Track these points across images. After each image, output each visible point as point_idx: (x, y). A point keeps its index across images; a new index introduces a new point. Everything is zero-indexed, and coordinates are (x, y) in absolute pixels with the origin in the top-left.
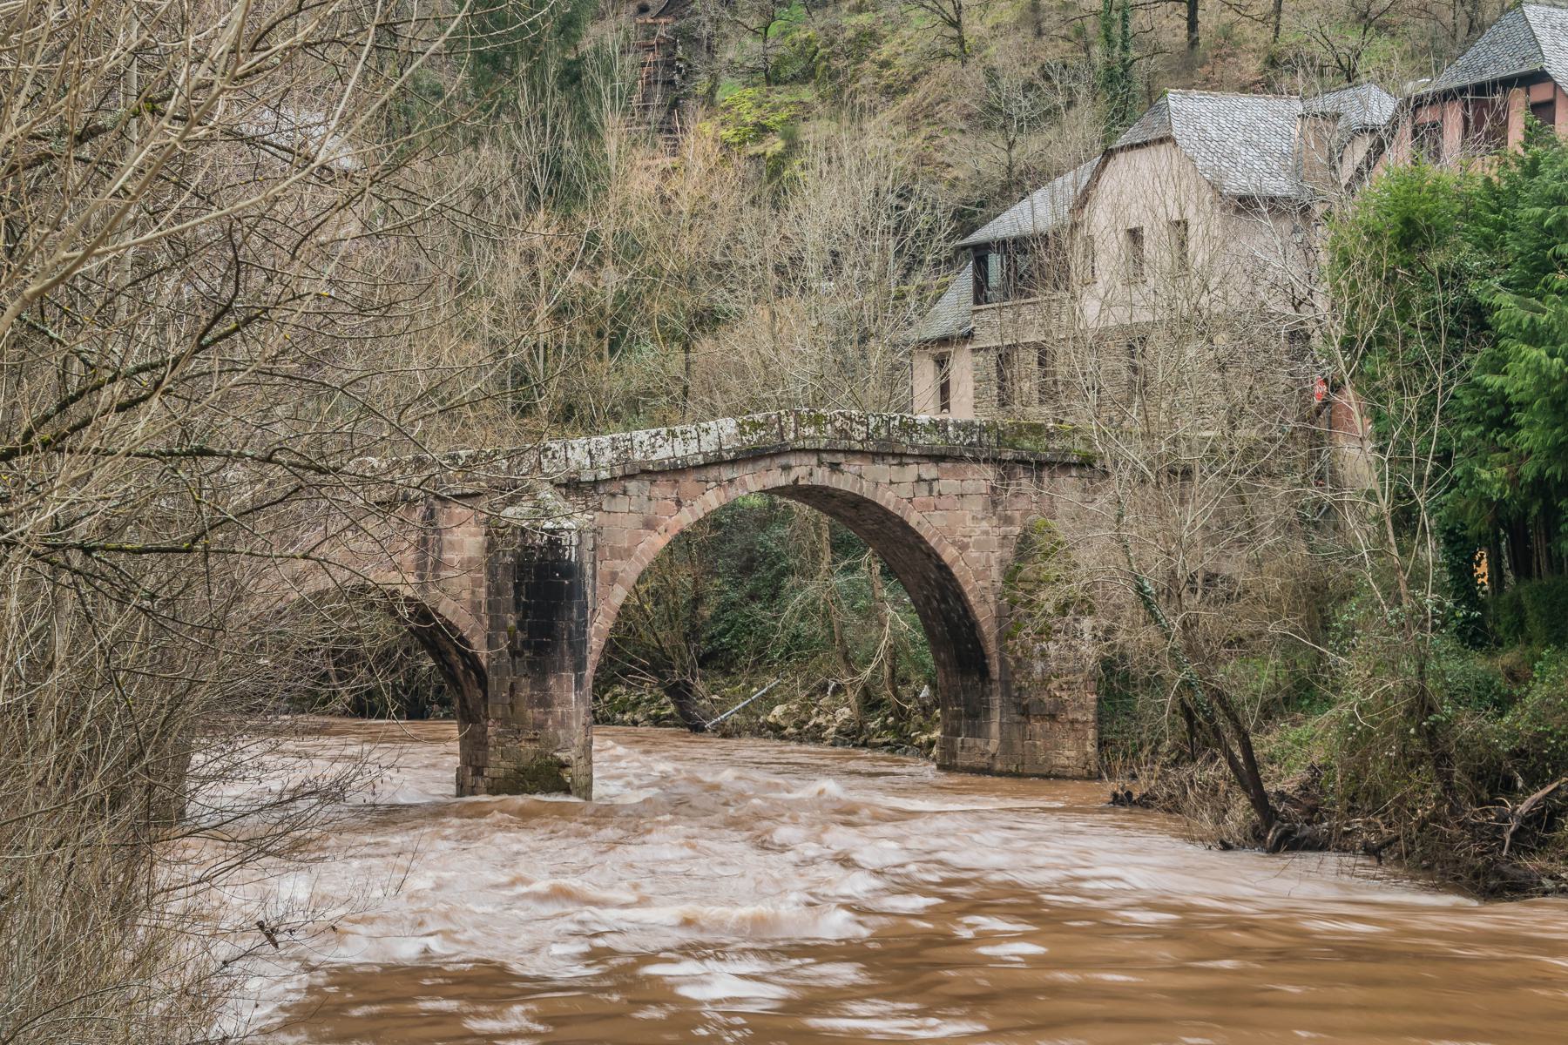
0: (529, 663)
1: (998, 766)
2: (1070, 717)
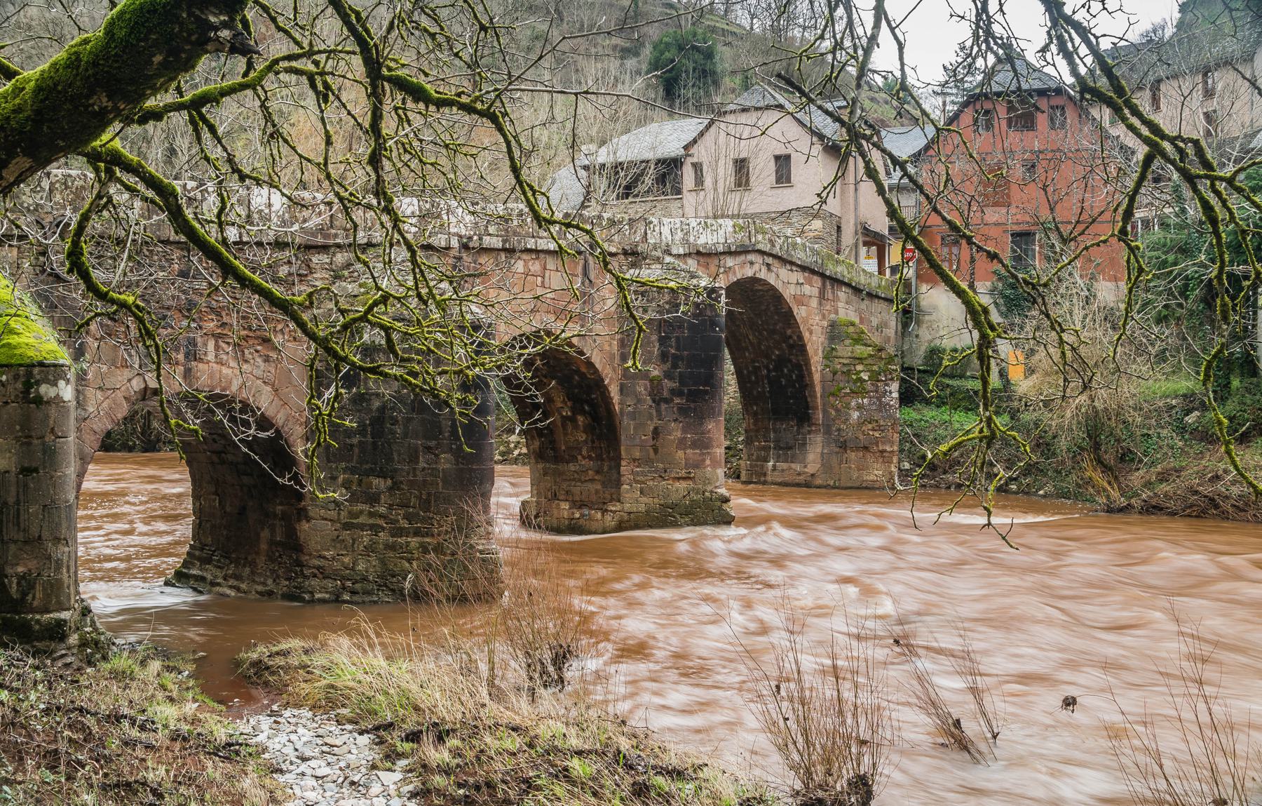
0: (679, 409)
1: (819, 482)
2: (881, 448)
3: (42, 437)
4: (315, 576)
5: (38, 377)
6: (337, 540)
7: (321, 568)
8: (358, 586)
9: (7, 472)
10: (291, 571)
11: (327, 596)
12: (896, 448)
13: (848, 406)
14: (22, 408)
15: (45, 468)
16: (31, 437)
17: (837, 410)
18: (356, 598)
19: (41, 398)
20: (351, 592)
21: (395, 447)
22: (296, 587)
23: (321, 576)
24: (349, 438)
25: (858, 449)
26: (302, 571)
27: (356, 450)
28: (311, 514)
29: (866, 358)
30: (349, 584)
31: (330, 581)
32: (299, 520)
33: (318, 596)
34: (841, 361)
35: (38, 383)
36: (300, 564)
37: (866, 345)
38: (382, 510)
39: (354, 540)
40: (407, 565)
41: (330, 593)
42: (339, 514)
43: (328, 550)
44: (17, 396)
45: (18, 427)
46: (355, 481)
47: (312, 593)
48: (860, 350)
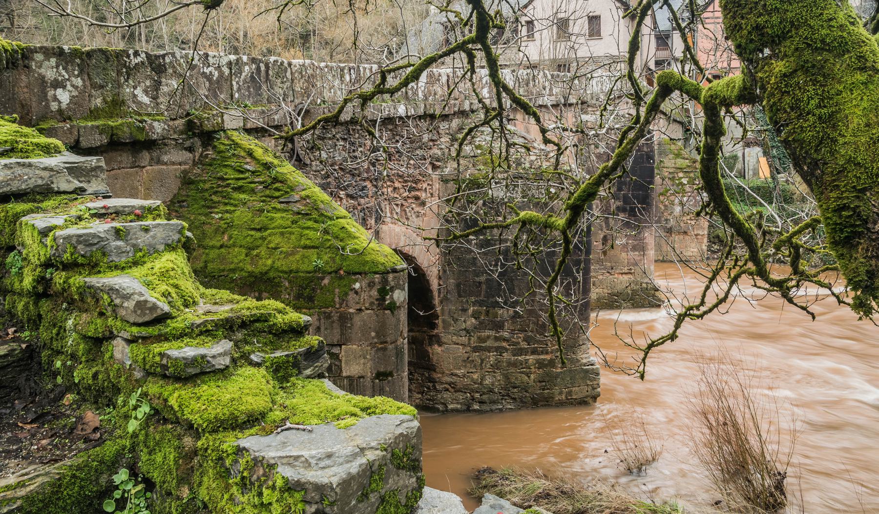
2: (696, 233)
3: (395, 342)
4: (447, 390)
5: (392, 284)
6: (467, 361)
7: (453, 383)
8: (485, 397)
9: (363, 377)
10: (423, 386)
11: (459, 406)
12: (706, 232)
13: (672, 203)
14: (377, 316)
15: (398, 370)
16: (386, 342)
17: (665, 206)
18: (485, 407)
19: (395, 303)
20: (480, 402)
21: (516, 283)
22: (429, 400)
23: (453, 390)
24: (477, 277)
25: (679, 233)
26: (434, 386)
27: (484, 287)
28: (443, 340)
29: (685, 168)
30: (477, 395)
31: (461, 393)
32: (431, 345)
33: (450, 407)
34: (668, 170)
35: (392, 289)
36: (433, 381)
37: (684, 158)
38: (506, 334)
39: (482, 361)
40: (526, 378)
41: (461, 404)
42: (469, 339)
43: (460, 369)
44: (372, 304)
45: (373, 334)
46: (484, 312)
47: (445, 404)
48: (680, 162)
